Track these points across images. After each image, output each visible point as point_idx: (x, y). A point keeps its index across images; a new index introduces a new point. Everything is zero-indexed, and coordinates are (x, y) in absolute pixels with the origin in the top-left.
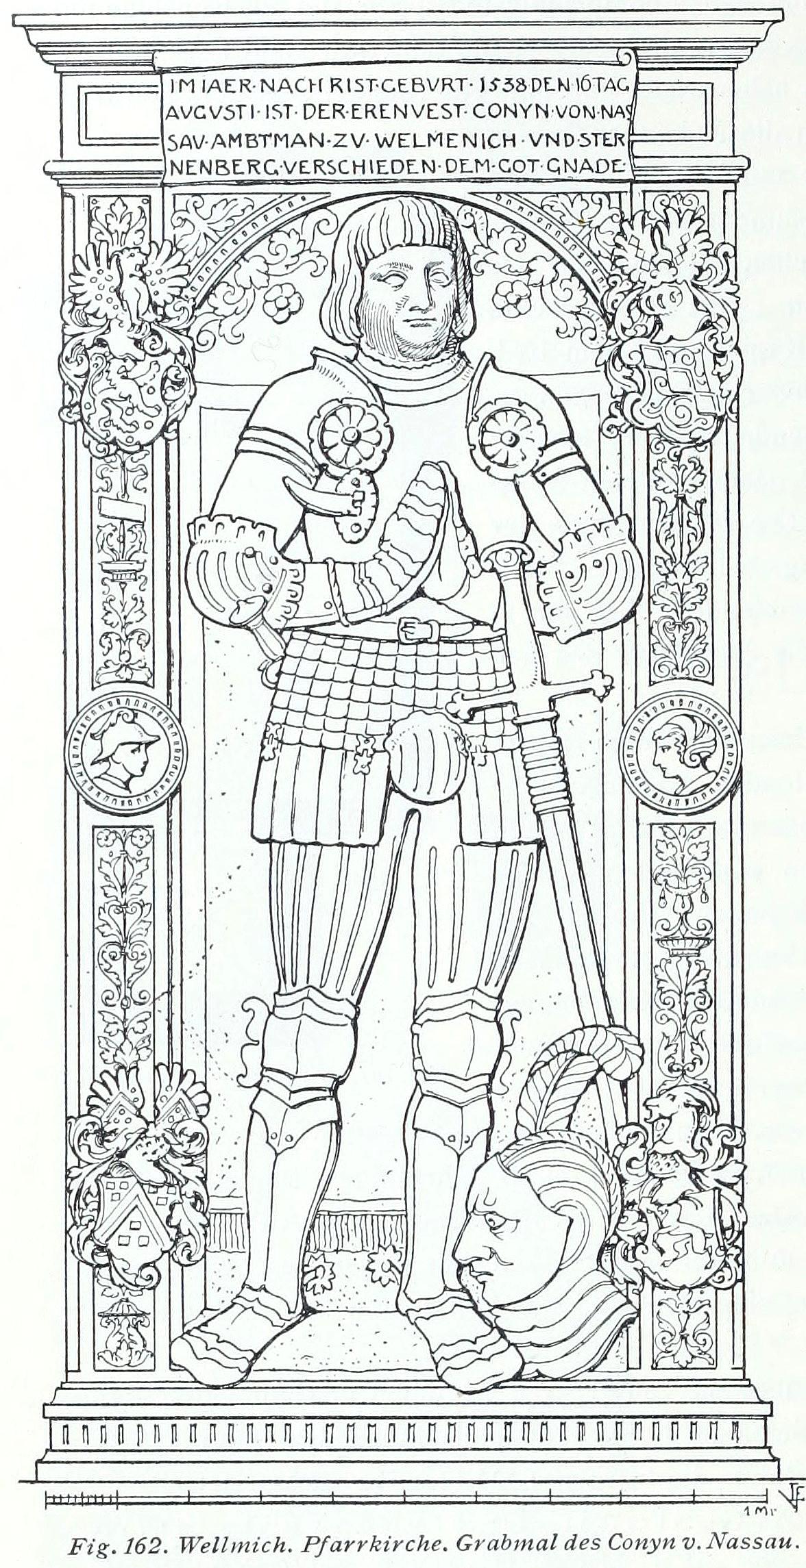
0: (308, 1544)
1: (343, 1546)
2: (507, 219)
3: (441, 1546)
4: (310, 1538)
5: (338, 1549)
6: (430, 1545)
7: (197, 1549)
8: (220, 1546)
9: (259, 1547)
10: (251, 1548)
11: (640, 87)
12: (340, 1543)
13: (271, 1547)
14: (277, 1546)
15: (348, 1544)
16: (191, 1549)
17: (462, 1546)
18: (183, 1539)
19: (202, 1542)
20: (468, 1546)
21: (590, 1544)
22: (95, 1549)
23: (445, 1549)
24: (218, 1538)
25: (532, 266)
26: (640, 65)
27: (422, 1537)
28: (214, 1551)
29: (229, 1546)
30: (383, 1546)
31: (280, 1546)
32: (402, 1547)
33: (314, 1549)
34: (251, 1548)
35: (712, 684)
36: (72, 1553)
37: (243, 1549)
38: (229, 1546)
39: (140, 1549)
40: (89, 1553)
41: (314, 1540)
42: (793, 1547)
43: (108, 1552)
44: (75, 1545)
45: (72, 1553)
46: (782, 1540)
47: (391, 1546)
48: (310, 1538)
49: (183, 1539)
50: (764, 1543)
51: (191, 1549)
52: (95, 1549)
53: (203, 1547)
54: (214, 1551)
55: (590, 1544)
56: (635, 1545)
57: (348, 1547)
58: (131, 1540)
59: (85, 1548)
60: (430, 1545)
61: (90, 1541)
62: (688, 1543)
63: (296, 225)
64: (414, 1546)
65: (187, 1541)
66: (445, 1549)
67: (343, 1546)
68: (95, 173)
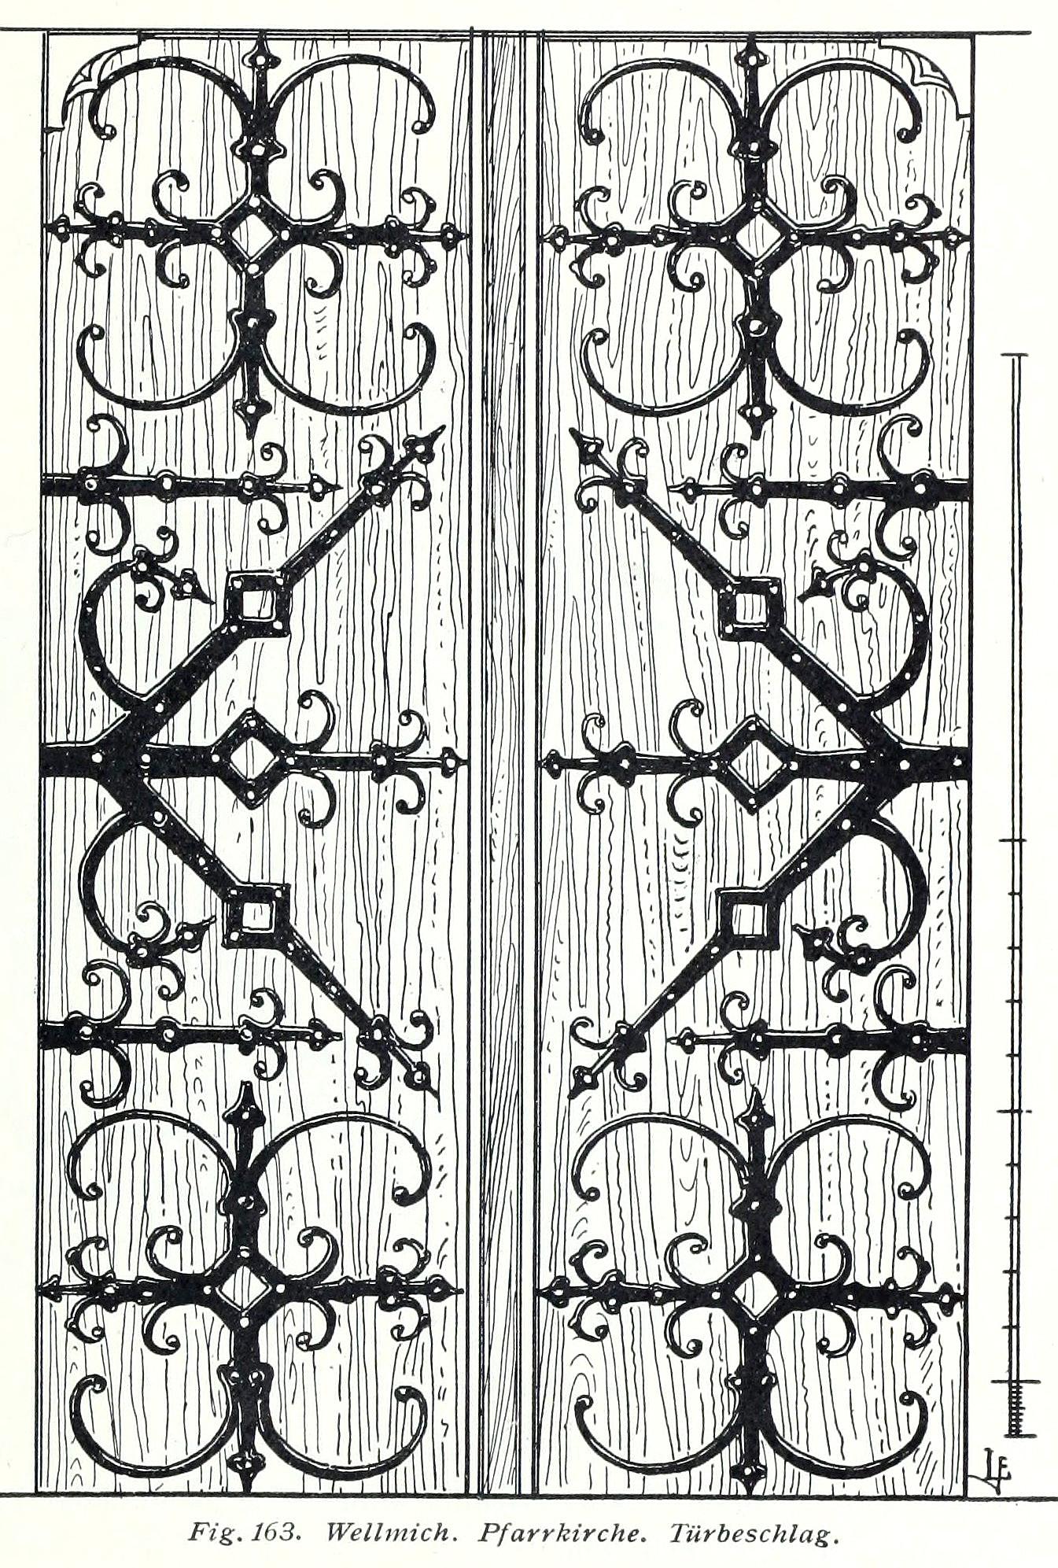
0: (486, 1531)
1: (526, 1535)
3: (639, 1537)
4: (488, 1525)
5: (520, 1539)
6: (625, 1536)
8: (372, 1534)
9: (418, 1535)
10: (409, 1535)
11: (890, 1493)
12: (522, 1532)
13: (770, 1536)
14: (438, 1533)
15: (588, 1533)
18: (331, 1525)
21: (745, 1536)
22: (218, 1535)
24: (371, 1525)
26: (527, 1489)
27: (617, 1526)
29: (383, 1534)
30: (571, 1535)
31: (442, 1533)
32: (594, 1537)
33: (493, 1538)
34: (409, 1535)
36: (193, 1538)
38: (383, 1534)
39: (271, 1534)
41: (492, 1528)
42: (450, 1540)
44: (195, 1531)
47: (581, 1535)
49: (331, 1525)
50: (758, 1535)
53: (353, 1535)
54: (366, 1538)
55: (745, 1535)
57: (532, 1535)
58: (260, 1526)
60: (625, 1536)
61: (213, 1526)
64: (607, 1536)
65: (336, 1527)
67: (526, 1535)
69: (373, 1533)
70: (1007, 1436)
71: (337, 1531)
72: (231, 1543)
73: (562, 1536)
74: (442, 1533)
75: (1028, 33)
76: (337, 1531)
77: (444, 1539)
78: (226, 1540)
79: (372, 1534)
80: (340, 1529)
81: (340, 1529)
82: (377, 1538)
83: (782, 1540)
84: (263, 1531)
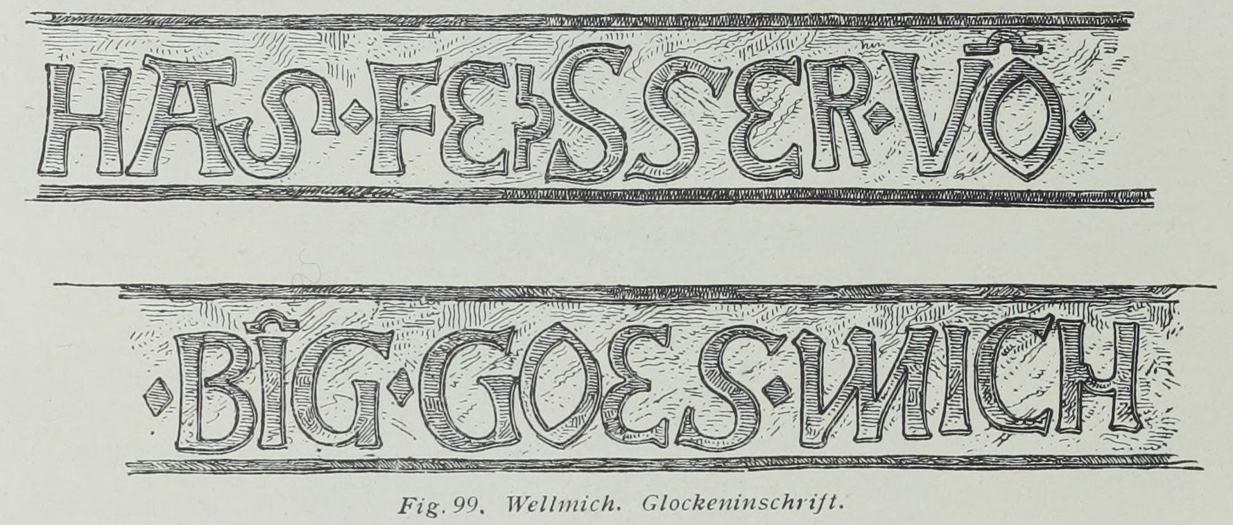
2: (751, 464)
7: (525, 508)
8: (548, 505)
9: (588, 506)
13: (690, 505)
14: (605, 505)
16: (519, 507)
17: (648, 506)
22: (425, 509)
23: (482, 512)
28: (542, 510)
29: (557, 506)
31: (608, 505)
35: (355, 101)
36: (402, 512)
37: (725, 507)
38: (557, 506)
43: (437, 510)
44: (405, 504)
45: (402, 512)
46: (791, 507)
48: (406, 499)
51: (519, 507)
59: (415, 506)
61: (420, 501)
62: (788, 502)
66: (482, 512)
69: (547, 505)
70: (1131, 15)
71: (516, 503)
72: (436, 515)
73: (698, 505)
74: (608, 505)
75: (1140, 199)
76: (516, 503)
77: (610, 509)
78: (432, 513)
79: (548, 505)
80: (519, 501)
81: (519, 501)
82: (583, 510)
83: (791, 507)
84: (460, 504)
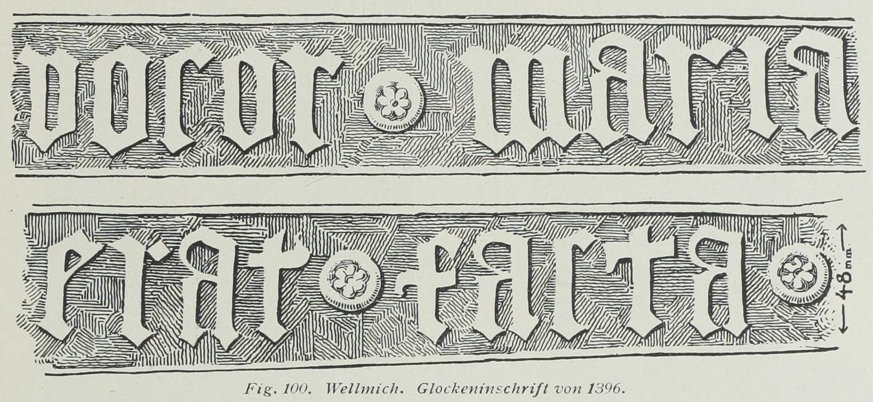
7: (338, 391)
8: (354, 390)
9: (381, 390)
13: (388, 390)
15: (524, 388)
19: (342, 386)
20: (425, 390)
22: (262, 391)
25: (846, 248)
28: (350, 392)
29: (360, 390)
31: (394, 389)
38: (360, 390)
40: (259, 392)
52: (262, 391)
56: (572, 390)
63: (681, 225)
65: (332, 386)
68: (119, 215)
